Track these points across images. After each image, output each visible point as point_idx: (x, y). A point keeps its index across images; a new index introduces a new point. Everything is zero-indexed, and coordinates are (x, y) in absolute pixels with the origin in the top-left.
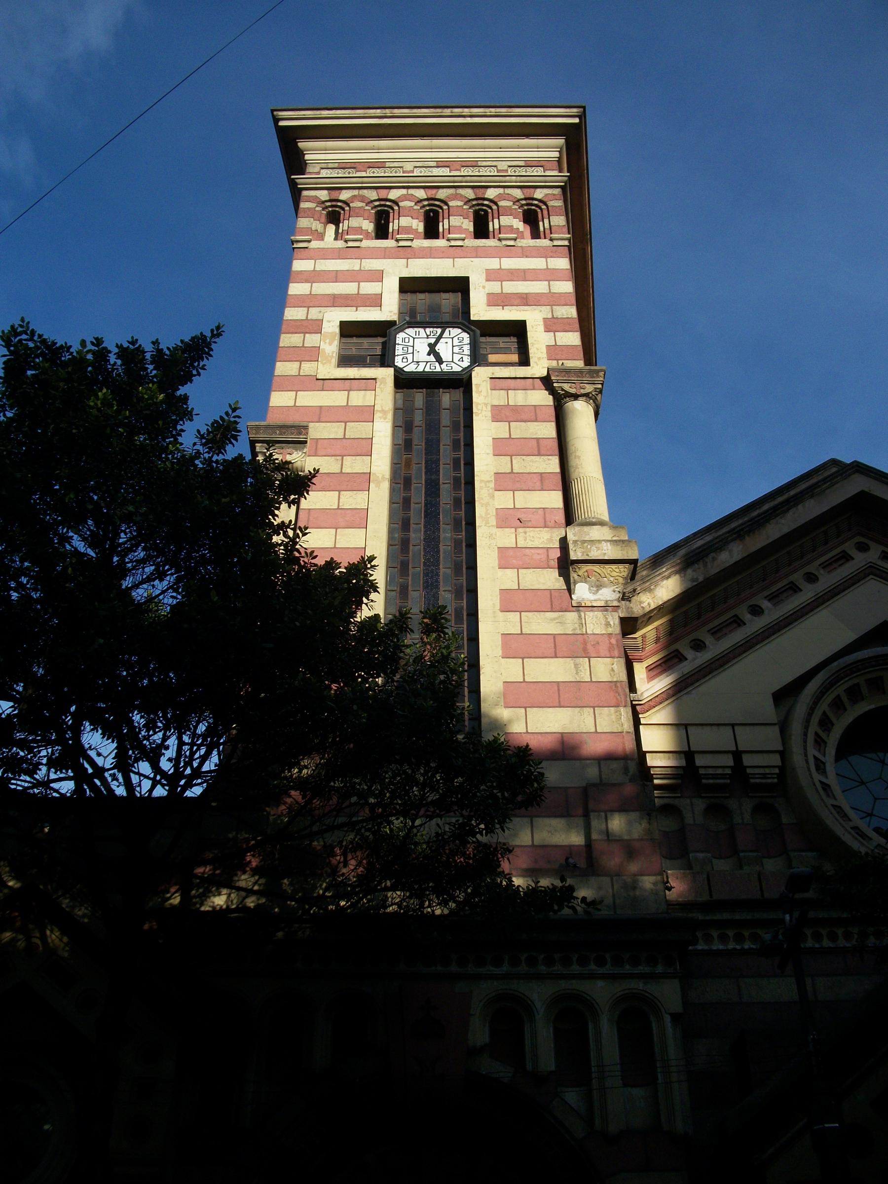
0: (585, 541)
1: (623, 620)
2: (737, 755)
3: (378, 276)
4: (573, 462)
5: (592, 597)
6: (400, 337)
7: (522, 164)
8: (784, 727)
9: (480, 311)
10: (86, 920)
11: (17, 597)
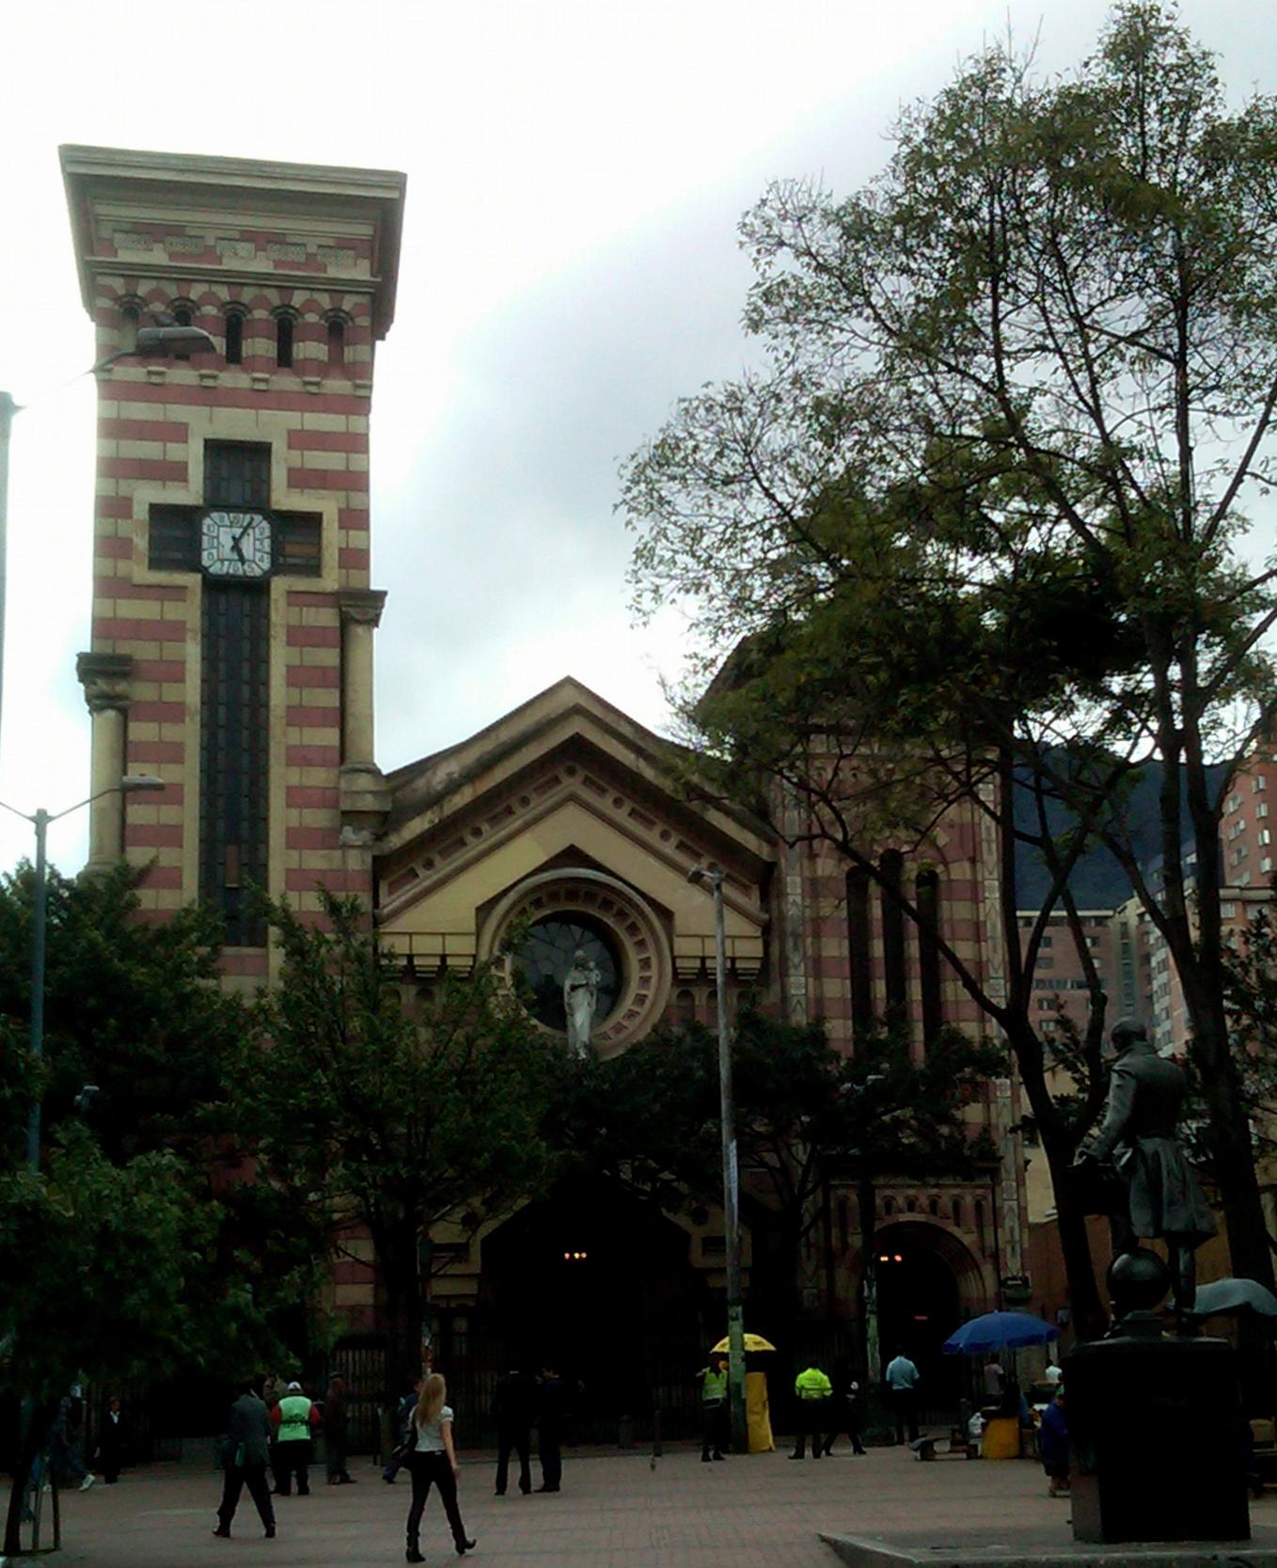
2: (443, 957)
3: (179, 433)
4: (351, 695)
5: (354, 837)
7: (332, 243)
8: (478, 934)
9: (284, 498)
11: (332, 1138)
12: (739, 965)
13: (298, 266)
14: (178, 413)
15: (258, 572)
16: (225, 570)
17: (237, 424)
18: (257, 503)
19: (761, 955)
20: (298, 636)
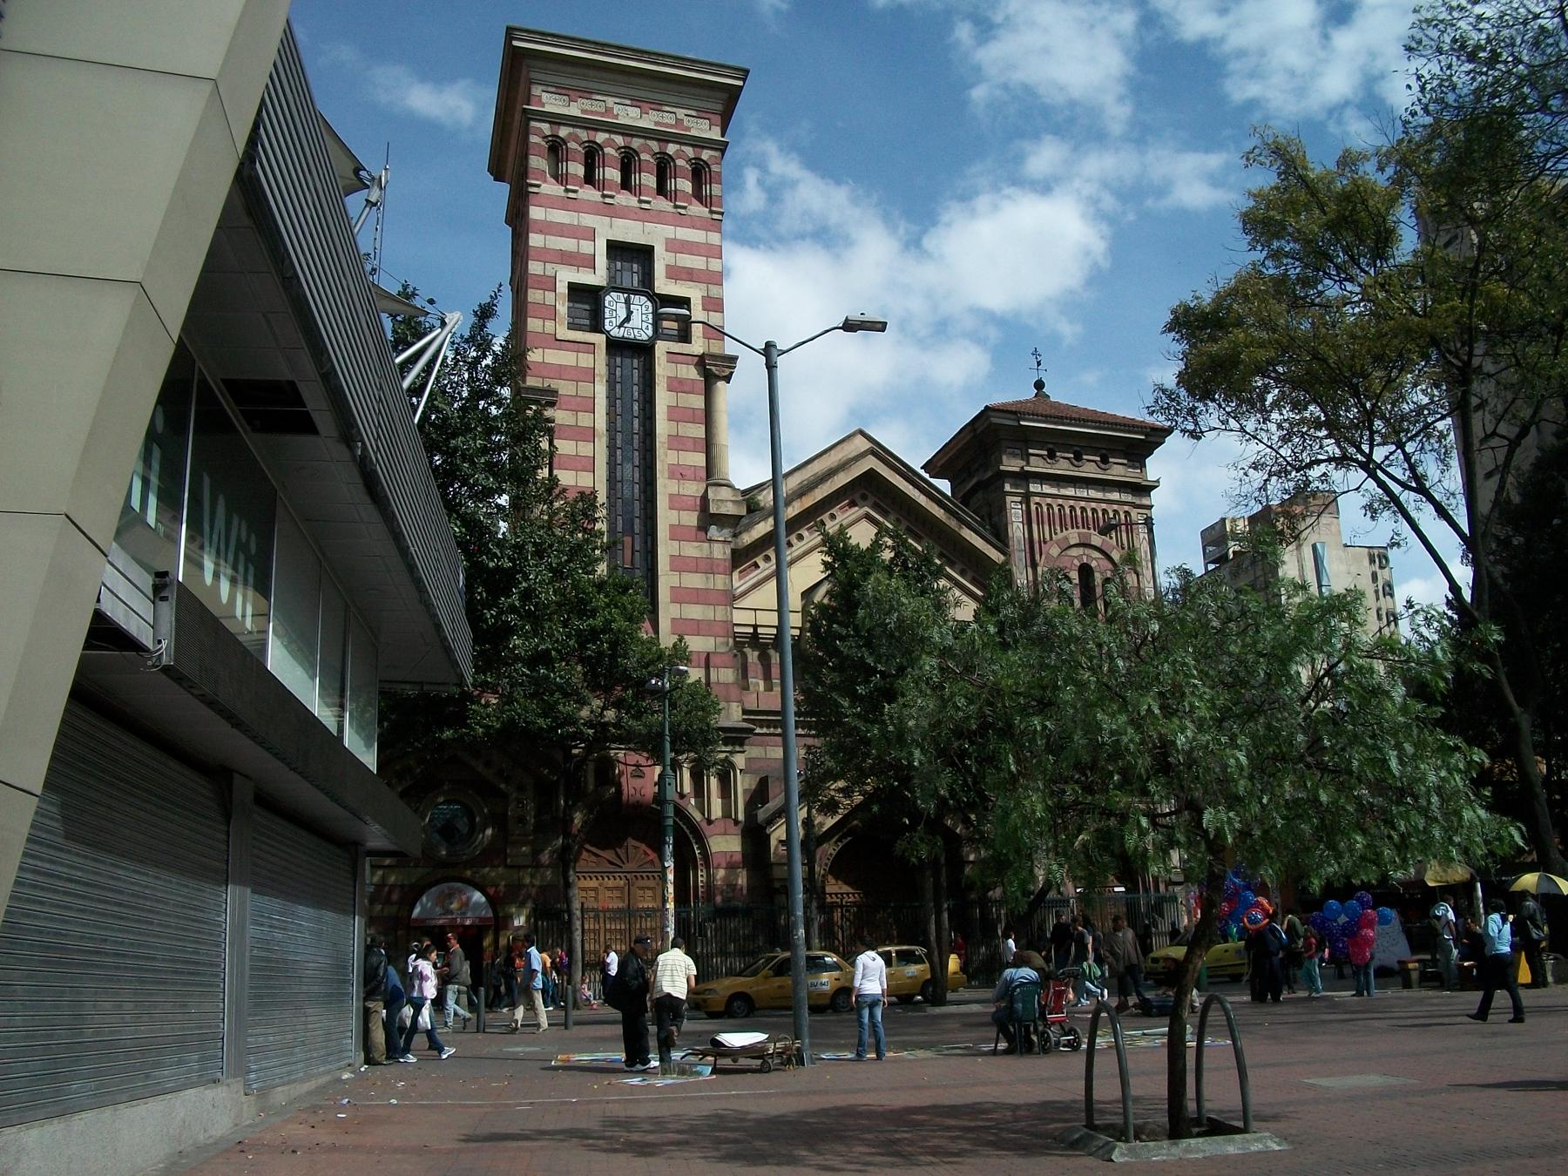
0: (718, 500)
1: (734, 551)
3: (591, 235)
6: (608, 298)
9: (663, 286)
10: (386, 724)
12: (760, 630)
13: (671, 126)
14: (588, 220)
15: (645, 337)
16: (621, 335)
17: (631, 232)
18: (646, 286)
19: (776, 624)
20: (676, 385)
